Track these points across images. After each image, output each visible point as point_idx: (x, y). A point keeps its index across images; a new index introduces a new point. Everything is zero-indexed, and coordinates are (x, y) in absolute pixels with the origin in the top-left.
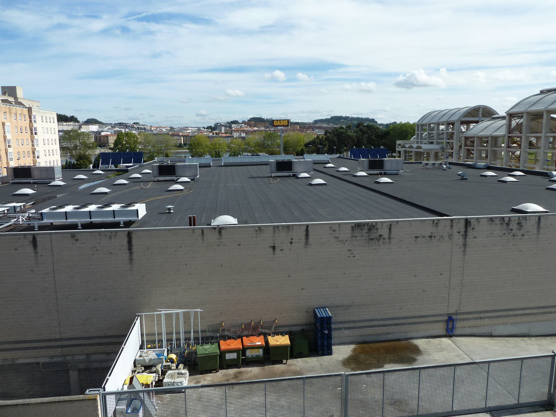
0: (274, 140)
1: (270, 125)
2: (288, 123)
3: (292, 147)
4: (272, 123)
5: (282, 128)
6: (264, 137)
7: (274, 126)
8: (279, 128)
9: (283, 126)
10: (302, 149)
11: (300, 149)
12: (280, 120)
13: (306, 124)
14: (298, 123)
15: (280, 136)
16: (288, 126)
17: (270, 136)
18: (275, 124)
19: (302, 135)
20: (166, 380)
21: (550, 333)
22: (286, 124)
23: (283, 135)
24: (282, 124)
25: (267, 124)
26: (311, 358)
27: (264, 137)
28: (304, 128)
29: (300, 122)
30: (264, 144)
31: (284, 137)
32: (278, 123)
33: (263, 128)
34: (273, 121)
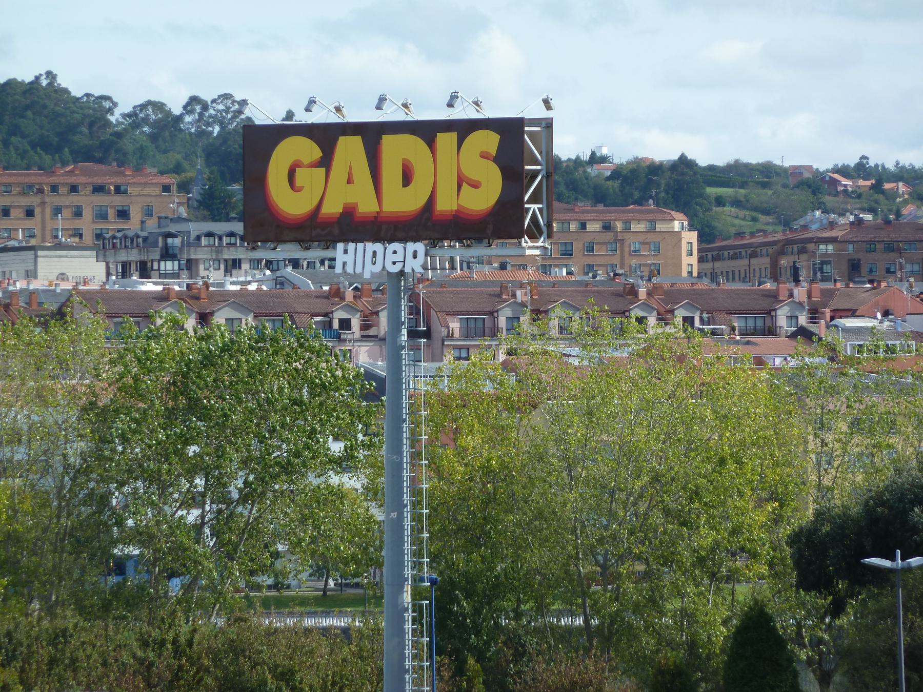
0: (268, 473)
1: (211, 206)
2: (521, 178)
3: (576, 591)
4: (232, 168)
5: (409, 257)
6: (98, 416)
7: (266, 227)
8: (359, 260)
9: (427, 226)
10: (755, 629)
11: (716, 619)
12: (372, 134)
13: (815, 186)
14: (675, 185)
15: (375, 389)
16: (504, 222)
17: (195, 401)
18: (291, 203)
19: (747, 373)
20: (727, 209)
21: (12, 254)
22: (484, 197)
23: (421, 379)
24: (402, 201)
25: (151, 198)
26: (465, 117)
27: (98, 416)
28: (787, 255)
29: (708, 152)
30: (89, 538)
31: (448, 410)
32: (346, 187)
33: (85, 270)
34: (260, 140)
